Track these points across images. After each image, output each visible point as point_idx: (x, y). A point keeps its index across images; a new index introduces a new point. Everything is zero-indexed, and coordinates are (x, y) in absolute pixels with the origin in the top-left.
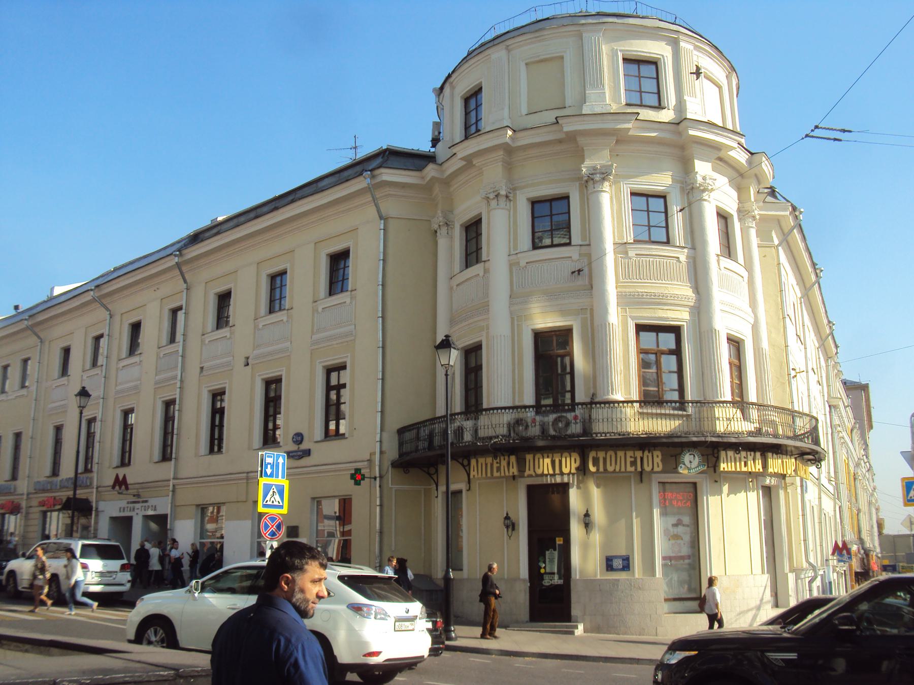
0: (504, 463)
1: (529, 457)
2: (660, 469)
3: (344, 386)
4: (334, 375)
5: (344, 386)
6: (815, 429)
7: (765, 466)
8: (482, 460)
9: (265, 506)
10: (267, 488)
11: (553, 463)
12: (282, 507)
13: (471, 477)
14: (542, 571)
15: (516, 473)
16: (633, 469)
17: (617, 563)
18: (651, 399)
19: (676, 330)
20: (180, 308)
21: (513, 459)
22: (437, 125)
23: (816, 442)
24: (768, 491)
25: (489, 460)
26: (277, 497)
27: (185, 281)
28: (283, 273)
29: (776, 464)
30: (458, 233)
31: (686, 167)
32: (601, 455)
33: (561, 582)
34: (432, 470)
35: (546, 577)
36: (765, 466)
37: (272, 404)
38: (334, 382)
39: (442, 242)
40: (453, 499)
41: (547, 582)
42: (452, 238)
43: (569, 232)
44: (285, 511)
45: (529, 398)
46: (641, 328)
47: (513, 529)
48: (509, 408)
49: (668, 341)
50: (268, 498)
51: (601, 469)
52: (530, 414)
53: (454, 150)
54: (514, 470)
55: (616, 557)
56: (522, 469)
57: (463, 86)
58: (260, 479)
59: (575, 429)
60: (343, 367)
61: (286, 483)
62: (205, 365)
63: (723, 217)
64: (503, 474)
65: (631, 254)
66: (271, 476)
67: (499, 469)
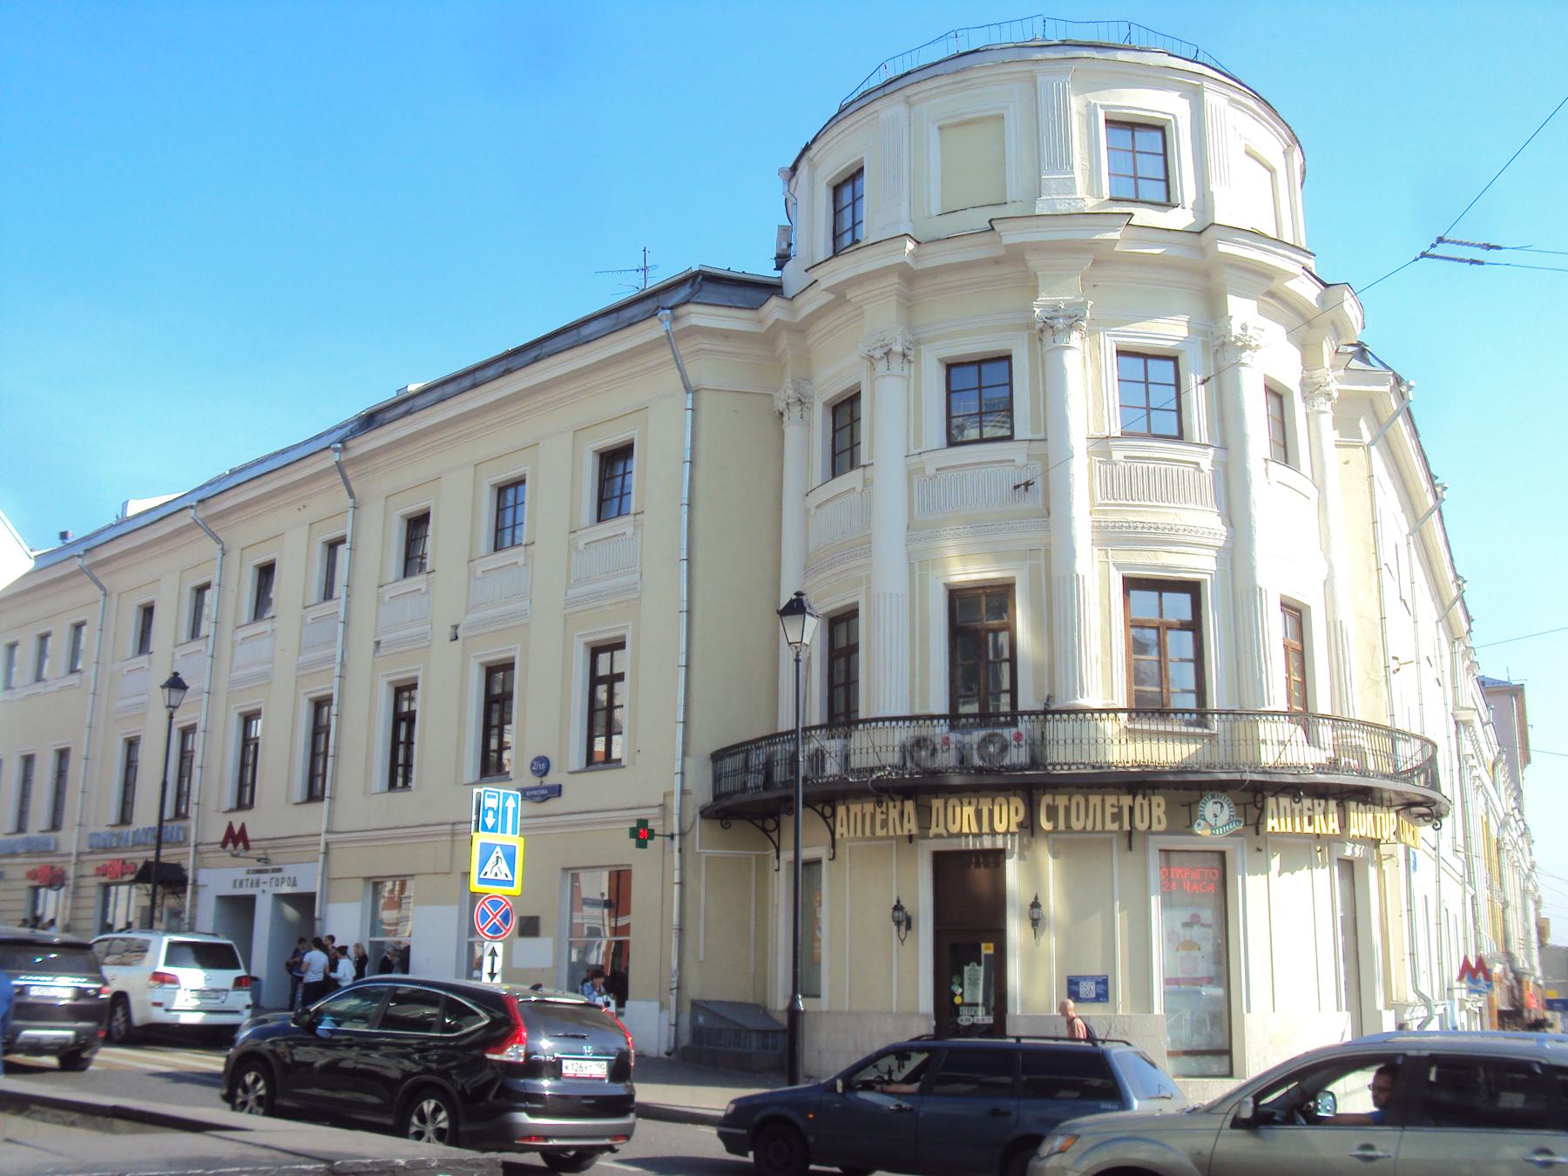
0: (894, 813)
1: (937, 804)
2: (1163, 827)
3: (620, 677)
5: (620, 677)
6: (1432, 760)
7: (1344, 824)
8: (855, 808)
9: (482, 881)
10: (487, 850)
11: (978, 814)
12: (511, 883)
13: (837, 836)
14: (958, 1000)
15: (914, 831)
16: (1115, 827)
17: (1087, 989)
18: (1148, 708)
20: (342, 540)
23: (1434, 784)
26: (503, 866)
27: (351, 495)
28: (519, 483)
29: (1362, 821)
30: (819, 419)
32: (1061, 801)
34: (770, 824)
35: (964, 1011)
36: (1344, 824)
37: (496, 707)
39: (792, 432)
44: (516, 890)
47: (909, 927)
48: (904, 719)
49: (1178, 607)
50: (488, 868)
51: (1062, 826)
52: (940, 730)
53: (815, 274)
54: (911, 826)
55: (1085, 978)
56: (924, 825)
57: (831, 163)
59: (1018, 756)
60: (620, 645)
61: (518, 842)
62: (384, 638)
64: (891, 833)
66: (494, 829)
67: (884, 824)
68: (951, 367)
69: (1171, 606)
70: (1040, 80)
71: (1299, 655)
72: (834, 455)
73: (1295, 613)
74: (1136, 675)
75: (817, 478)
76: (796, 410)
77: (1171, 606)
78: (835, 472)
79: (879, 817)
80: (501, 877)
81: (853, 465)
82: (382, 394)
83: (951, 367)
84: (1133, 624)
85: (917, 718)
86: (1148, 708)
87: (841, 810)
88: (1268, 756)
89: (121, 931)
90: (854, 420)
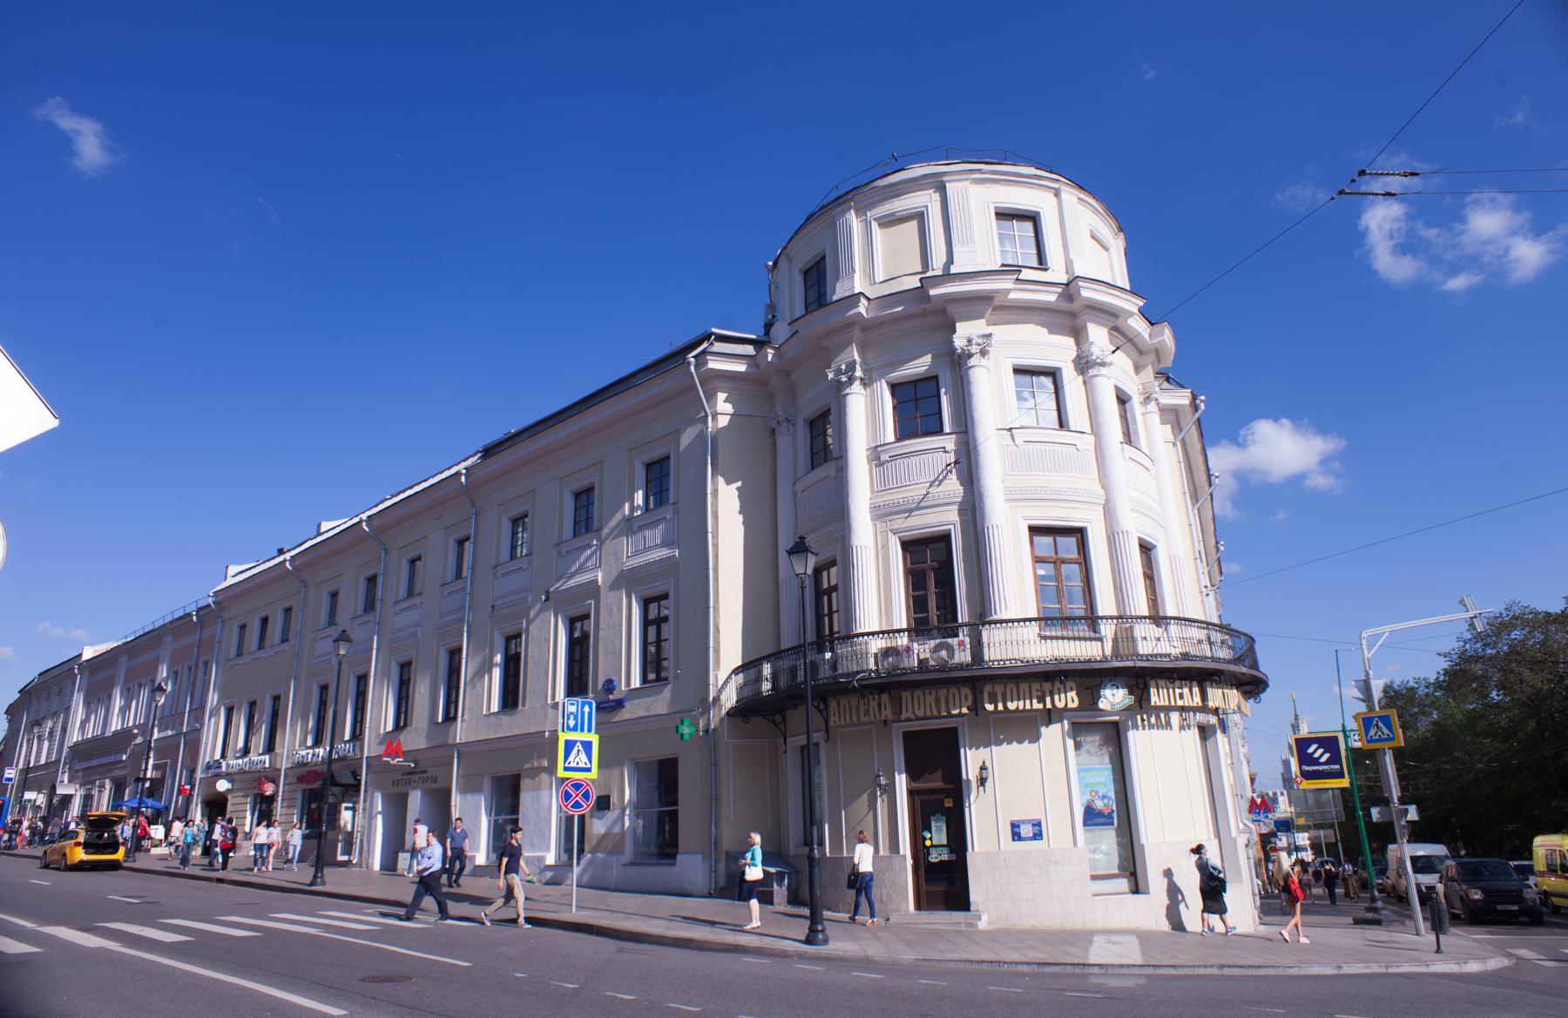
0: (874, 704)
1: (906, 695)
2: (1075, 704)
3: (666, 619)
4: (653, 607)
5: (666, 619)
6: (1252, 649)
7: (1204, 697)
8: (844, 701)
9: (566, 769)
10: (570, 745)
11: (937, 701)
12: (589, 770)
13: (831, 723)
14: (928, 843)
15: (890, 717)
16: (1040, 706)
17: (1026, 830)
18: (1052, 620)
19: (1079, 533)
20: (468, 539)
21: (885, 698)
22: (772, 307)
23: (1255, 666)
24: (1205, 732)
25: (854, 701)
26: (583, 757)
27: (473, 505)
28: (590, 489)
29: (1216, 696)
30: (802, 432)
31: (1078, 334)
33: (954, 857)
34: (778, 718)
36: (1204, 697)
37: (577, 648)
38: (652, 615)
39: (783, 441)
40: (808, 756)
41: (934, 857)
42: (794, 437)
43: (710, 896)
44: (594, 774)
45: (901, 620)
46: (1035, 530)
48: (878, 633)
49: (1068, 545)
50: (571, 758)
52: (903, 640)
53: (796, 326)
54: (888, 713)
55: (1024, 822)
56: (898, 711)
57: (803, 256)
58: (560, 734)
59: (963, 656)
60: (665, 596)
61: (594, 739)
62: (498, 603)
63: (1123, 399)
65: (1019, 440)
66: (575, 729)
67: (867, 713)
68: (649, 466)
69: (1062, 542)
70: (948, 185)
71: (1150, 576)
72: (812, 455)
73: (1146, 549)
74: (1041, 591)
75: (801, 469)
76: (784, 425)
77: (1062, 542)
78: (813, 466)
79: (862, 708)
80: (582, 765)
81: (588, 530)
82: (497, 435)
83: (649, 466)
84: (1038, 560)
85: (888, 632)
86: (1052, 620)
87: (833, 704)
88: (1144, 648)
89: (1541, 874)
90: (589, 504)
